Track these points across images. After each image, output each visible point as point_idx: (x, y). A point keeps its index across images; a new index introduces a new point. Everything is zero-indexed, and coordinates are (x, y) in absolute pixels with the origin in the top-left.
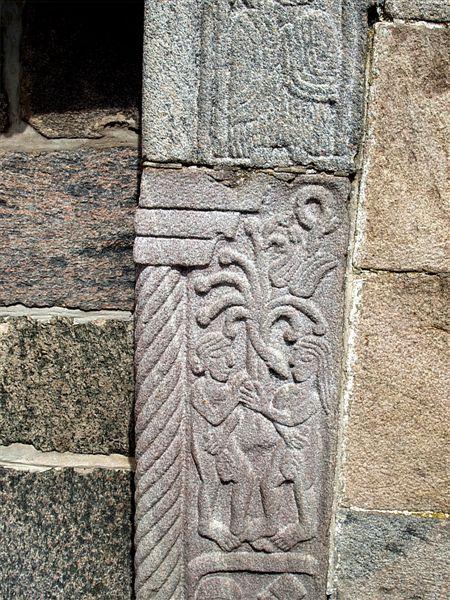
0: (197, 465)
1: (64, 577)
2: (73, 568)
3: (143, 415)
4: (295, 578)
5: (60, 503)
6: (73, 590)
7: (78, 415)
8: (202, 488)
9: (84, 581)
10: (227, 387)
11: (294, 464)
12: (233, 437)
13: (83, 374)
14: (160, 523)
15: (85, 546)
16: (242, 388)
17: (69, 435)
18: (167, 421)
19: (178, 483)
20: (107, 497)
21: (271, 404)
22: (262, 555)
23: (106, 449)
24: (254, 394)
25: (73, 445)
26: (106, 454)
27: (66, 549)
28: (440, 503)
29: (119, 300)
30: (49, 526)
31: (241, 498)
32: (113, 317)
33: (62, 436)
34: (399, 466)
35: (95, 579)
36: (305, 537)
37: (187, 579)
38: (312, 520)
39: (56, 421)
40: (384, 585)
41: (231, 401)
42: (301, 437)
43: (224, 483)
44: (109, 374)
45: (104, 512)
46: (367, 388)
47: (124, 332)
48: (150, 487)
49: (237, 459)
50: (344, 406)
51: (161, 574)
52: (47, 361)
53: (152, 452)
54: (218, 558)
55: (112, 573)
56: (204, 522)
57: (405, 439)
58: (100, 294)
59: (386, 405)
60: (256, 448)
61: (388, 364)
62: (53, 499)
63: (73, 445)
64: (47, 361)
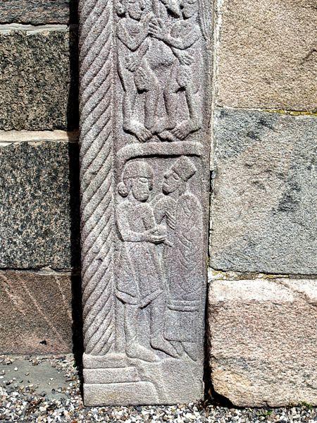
0: (121, 79)
1: (22, 225)
2: (28, 219)
3: (85, 44)
4: (188, 159)
5: (18, 169)
6: (28, 236)
7: (31, 101)
8: (125, 96)
9: (36, 228)
10: (140, 24)
11: (185, 75)
12: (145, 59)
13: (33, 72)
14: (97, 123)
15: (37, 201)
16: (150, 24)
17: (25, 116)
18: (101, 48)
19: (108, 94)
20: (52, 162)
21: (169, 35)
22: (166, 143)
23: (51, 126)
24: (158, 27)
25: (27, 124)
26: (51, 130)
27: (23, 204)
28: (281, 102)
29: (59, 16)
30: (10, 187)
31: (151, 102)
32: (54, 29)
33: (19, 118)
34: (253, 77)
35: (44, 226)
36: (194, 128)
37: (116, 164)
38: (198, 115)
39: (15, 107)
40: (247, 162)
41: (143, 33)
42: (190, 56)
43: (140, 92)
44: (52, 71)
45: (50, 174)
46: (231, 22)
47: (63, 40)
48: (90, 96)
49: (148, 74)
50: (216, 35)
51: (99, 160)
52: (8, 63)
53: (91, 71)
54: (137, 147)
55: (56, 220)
56: (127, 120)
57: (256, 57)
58: (45, 12)
59: (244, 35)
60: (161, 66)
61: (243, 6)
62: (12, 166)
63: (27, 124)
64: (8, 63)
